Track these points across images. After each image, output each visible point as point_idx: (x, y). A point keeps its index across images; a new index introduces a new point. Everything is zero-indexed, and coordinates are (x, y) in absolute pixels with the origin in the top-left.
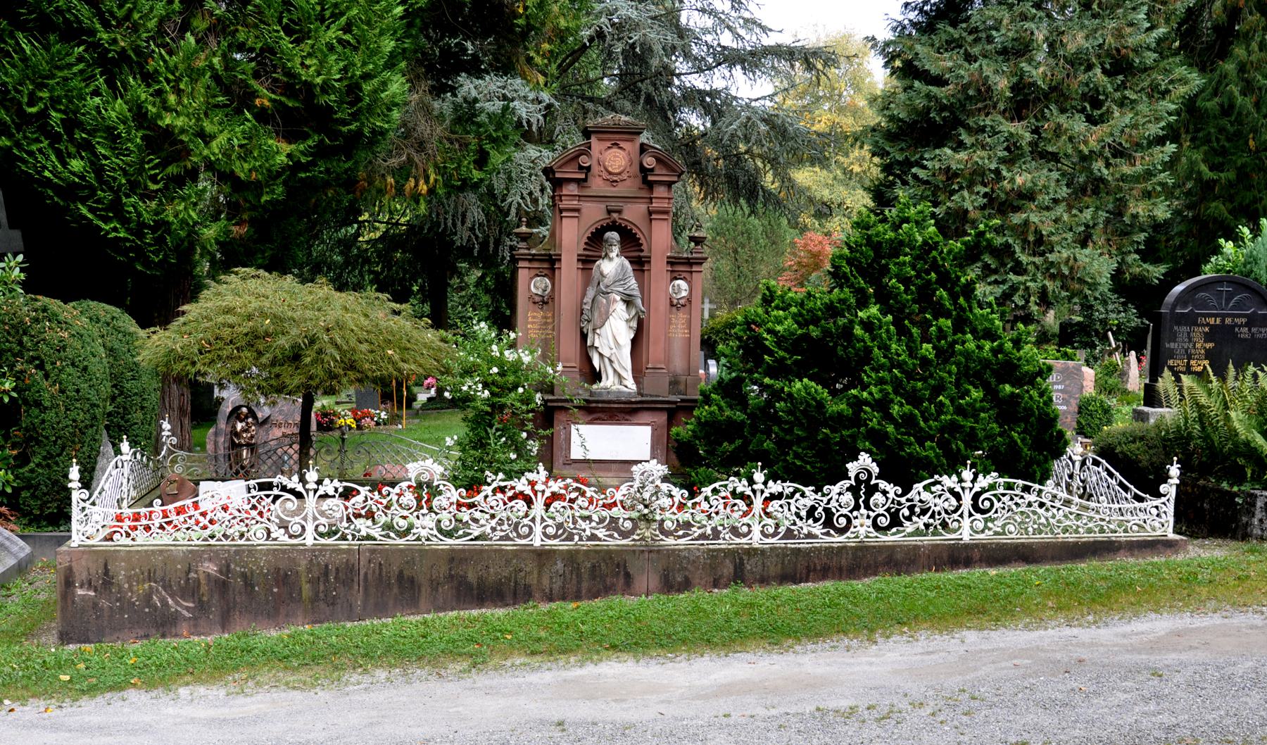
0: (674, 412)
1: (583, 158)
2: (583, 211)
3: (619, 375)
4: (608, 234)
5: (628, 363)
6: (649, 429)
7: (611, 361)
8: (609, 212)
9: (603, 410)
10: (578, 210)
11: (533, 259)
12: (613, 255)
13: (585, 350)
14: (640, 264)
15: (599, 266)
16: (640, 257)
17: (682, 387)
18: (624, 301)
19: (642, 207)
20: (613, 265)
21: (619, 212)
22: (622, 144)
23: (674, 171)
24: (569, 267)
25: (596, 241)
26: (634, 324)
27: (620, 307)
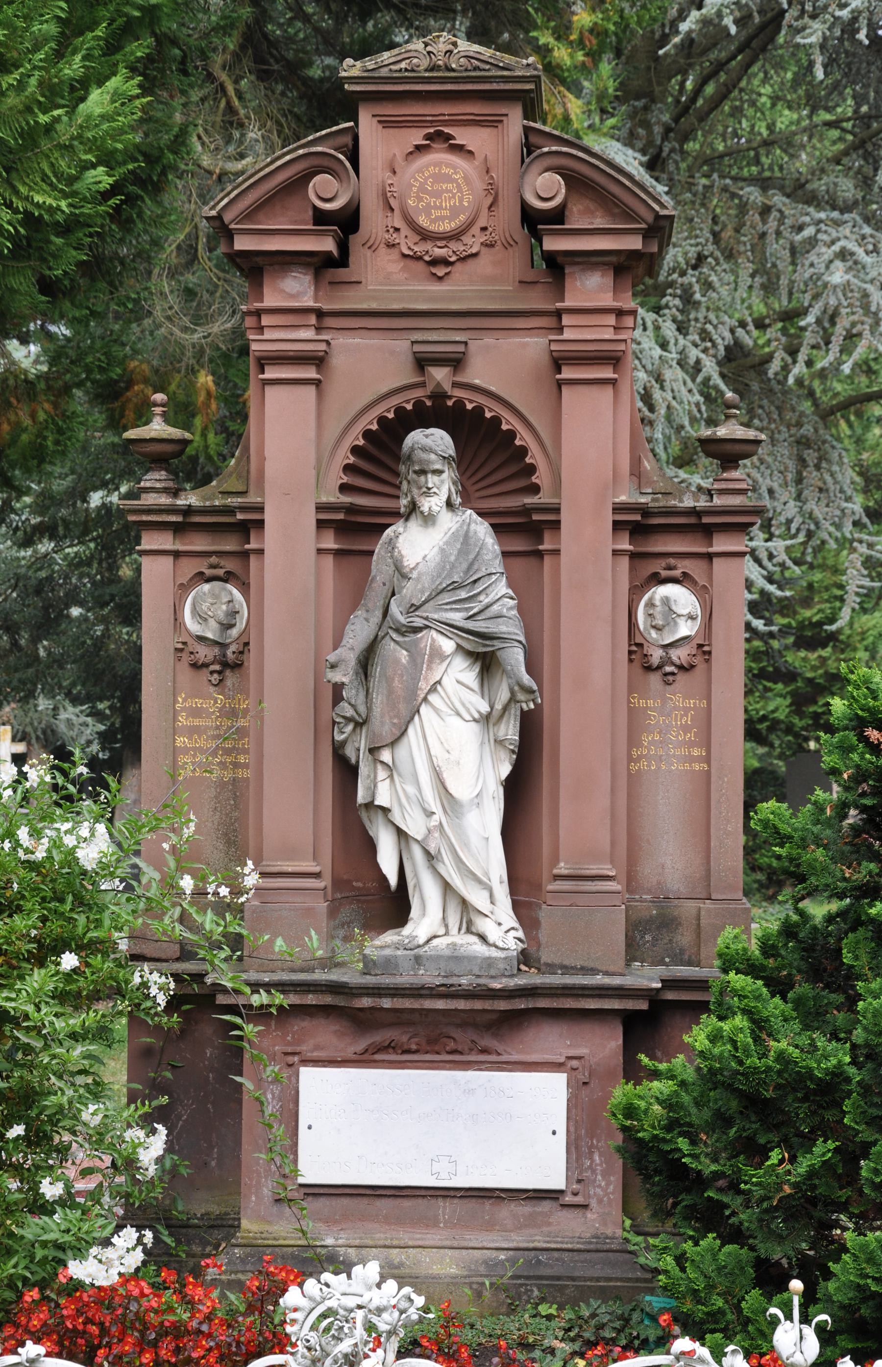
0: (646, 1024)
1: (322, 183)
2: (337, 361)
3: (464, 904)
4: (416, 437)
5: (493, 862)
6: (556, 1085)
7: (430, 857)
8: (422, 363)
9: (398, 1018)
10: (319, 361)
11: (185, 524)
12: (433, 503)
13: (353, 823)
14: (527, 532)
15: (391, 544)
16: (527, 511)
17: (684, 938)
18: (473, 656)
19: (532, 346)
20: (436, 535)
21: (456, 362)
22: (462, 136)
23: (629, 215)
24: (290, 541)
25: (380, 454)
26: (510, 731)
27: (458, 677)
